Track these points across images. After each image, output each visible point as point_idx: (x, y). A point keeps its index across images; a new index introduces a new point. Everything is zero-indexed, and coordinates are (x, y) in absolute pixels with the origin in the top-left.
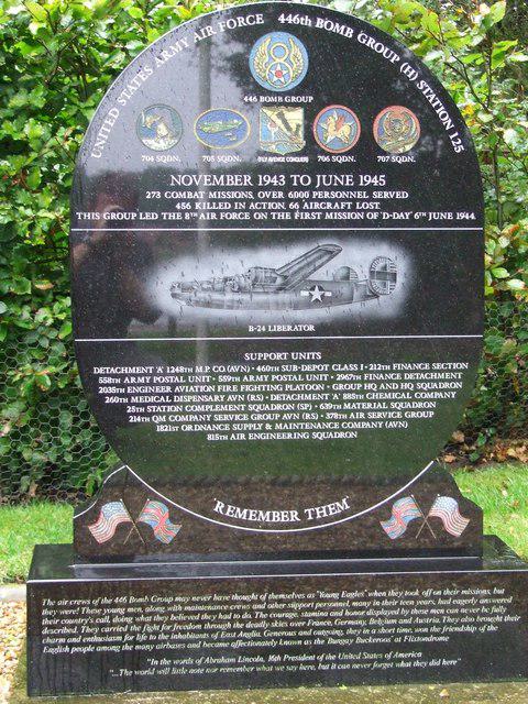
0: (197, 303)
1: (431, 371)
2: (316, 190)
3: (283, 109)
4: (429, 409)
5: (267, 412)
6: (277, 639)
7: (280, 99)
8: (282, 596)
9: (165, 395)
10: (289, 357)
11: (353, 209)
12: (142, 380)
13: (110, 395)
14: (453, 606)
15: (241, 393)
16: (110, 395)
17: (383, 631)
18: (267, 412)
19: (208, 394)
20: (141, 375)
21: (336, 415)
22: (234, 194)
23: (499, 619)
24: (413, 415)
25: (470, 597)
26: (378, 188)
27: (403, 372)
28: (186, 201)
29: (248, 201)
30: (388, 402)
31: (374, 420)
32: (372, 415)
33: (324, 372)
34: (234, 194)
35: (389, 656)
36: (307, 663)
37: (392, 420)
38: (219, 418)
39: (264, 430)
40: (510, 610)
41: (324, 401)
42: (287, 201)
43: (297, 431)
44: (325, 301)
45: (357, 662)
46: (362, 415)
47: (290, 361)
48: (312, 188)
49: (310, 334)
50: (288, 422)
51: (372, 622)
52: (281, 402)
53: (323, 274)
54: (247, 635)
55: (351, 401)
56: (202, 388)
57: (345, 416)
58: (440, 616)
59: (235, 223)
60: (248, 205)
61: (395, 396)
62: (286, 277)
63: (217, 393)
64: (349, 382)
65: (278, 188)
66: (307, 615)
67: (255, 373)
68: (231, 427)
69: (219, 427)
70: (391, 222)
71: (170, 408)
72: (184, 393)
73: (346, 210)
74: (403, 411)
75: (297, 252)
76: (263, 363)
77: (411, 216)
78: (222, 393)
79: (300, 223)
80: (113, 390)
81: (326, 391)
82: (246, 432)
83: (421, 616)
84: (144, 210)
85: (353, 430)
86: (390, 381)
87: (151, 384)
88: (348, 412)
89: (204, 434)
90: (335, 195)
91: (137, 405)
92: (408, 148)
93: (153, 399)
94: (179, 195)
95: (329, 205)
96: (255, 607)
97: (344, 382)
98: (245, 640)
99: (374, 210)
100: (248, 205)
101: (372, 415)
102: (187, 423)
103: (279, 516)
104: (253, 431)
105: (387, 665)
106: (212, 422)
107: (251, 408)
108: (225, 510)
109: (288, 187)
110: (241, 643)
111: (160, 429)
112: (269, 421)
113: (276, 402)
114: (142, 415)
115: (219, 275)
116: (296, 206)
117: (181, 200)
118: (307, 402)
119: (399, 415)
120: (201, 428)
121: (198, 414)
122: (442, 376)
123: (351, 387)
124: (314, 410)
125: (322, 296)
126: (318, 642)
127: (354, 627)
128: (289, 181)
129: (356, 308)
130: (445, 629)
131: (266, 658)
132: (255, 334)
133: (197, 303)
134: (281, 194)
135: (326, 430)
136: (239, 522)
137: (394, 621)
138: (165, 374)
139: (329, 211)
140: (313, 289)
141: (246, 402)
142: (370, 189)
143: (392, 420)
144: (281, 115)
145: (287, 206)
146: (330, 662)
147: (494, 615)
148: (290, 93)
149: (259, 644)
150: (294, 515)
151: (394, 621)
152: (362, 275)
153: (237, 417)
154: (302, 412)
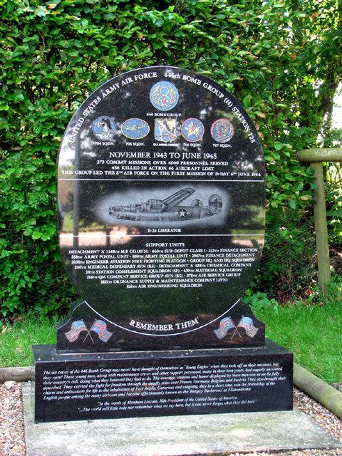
0: (122, 218)
1: (239, 252)
2: (183, 161)
3: (166, 119)
4: (238, 272)
5: (157, 274)
6: (164, 391)
7: (165, 115)
8: (167, 368)
9: (105, 264)
10: (168, 245)
11: (201, 170)
12: (93, 257)
13: (77, 265)
14: (253, 372)
15: (144, 264)
16: (77, 265)
17: (218, 386)
18: (157, 274)
19: (127, 264)
20: (93, 254)
21: (192, 275)
22: (141, 162)
23: (276, 379)
24: (230, 275)
25: (261, 368)
26: (213, 160)
27: (225, 253)
28: (117, 165)
29: (148, 166)
30: (218, 268)
31: (211, 278)
32: (210, 275)
33: (186, 253)
34: (141, 162)
35: (220, 399)
36: (179, 403)
37: (219, 277)
38: (132, 277)
39: (155, 283)
40: (282, 374)
41: (185, 268)
42: (168, 166)
43: (172, 283)
44: (186, 217)
45: (205, 402)
46: (205, 275)
47: (168, 247)
48: (180, 159)
49: (179, 233)
50: (167, 279)
51: (212, 381)
52: (164, 268)
53: (187, 203)
54: (149, 389)
55: (199, 268)
56: (124, 262)
57: (196, 276)
58: (246, 377)
59: (142, 177)
60: (148, 168)
61: (221, 265)
62: (167, 204)
63: (131, 263)
64: (199, 258)
65: (163, 160)
66: (180, 377)
67: (151, 254)
68: (139, 281)
69: (132, 282)
70: (219, 177)
71: (108, 272)
72: (114, 264)
73: (197, 171)
74: (225, 273)
75: (173, 191)
76: (155, 248)
77: (229, 174)
78: (134, 264)
79: (174, 177)
80: (78, 262)
81: (187, 263)
82: (147, 284)
83: (237, 378)
84: (96, 170)
85: (201, 283)
86: (219, 258)
87: (98, 259)
88: (198, 273)
89: (125, 285)
90: (191, 163)
91: (91, 270)
92: (228, 140)
93: (98, 267)
94: (114, 162)
95: (189, 168)
96: (153, 374)
97: (196, 258)
98: (148, 391)
99: (211, 171)
100: (148, 168)
101: (210, 275)
102: (117, 279)
103: (162, 328)
104: (150, 284)
105: (219, 404)
106: (129, 279)
107: (149, 271)
108: (135, 325)
109: (169, 159)
110: (146, 393)
111: (103, 282)
112: (158, 278)
113: (162, 268)
114: (93, 275)
115: (133, 203)
116: (172, 168)
117: (114, 165)
118: (177, 268)
119: (223, 275)
120: (123, 281)
121: (122, 274)
122: (244, 255)
123: (199, 260)
124: (181, 273)
125: (185, 214)
126: (185, 392)
127: (203, 384)
128: (169, 156)
129: (204, 220)
130: (250, 384)
131: (159, 401)
132: (151, 233)
133: (122, 218)
134: (165, 163)
135: (186, 283)
136: (142, 330)
137: (224, 381)
138: (105, 254)
139: (189, 171)
140: (180, 210)
141: (147, 269)
142: (209, 160)
143: (219, 277)
144: (165, 123)
145: (168, 168)
146: (191, 402)
147: (273, 377)
148: (169, 112)
149: (155, 393)
150: (170, 327)
151: (224, 381)
152: (206, 204)
153: (142, 276)
154: (174, 274)
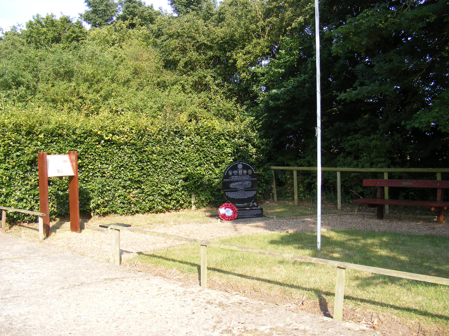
129: (247, 187)
